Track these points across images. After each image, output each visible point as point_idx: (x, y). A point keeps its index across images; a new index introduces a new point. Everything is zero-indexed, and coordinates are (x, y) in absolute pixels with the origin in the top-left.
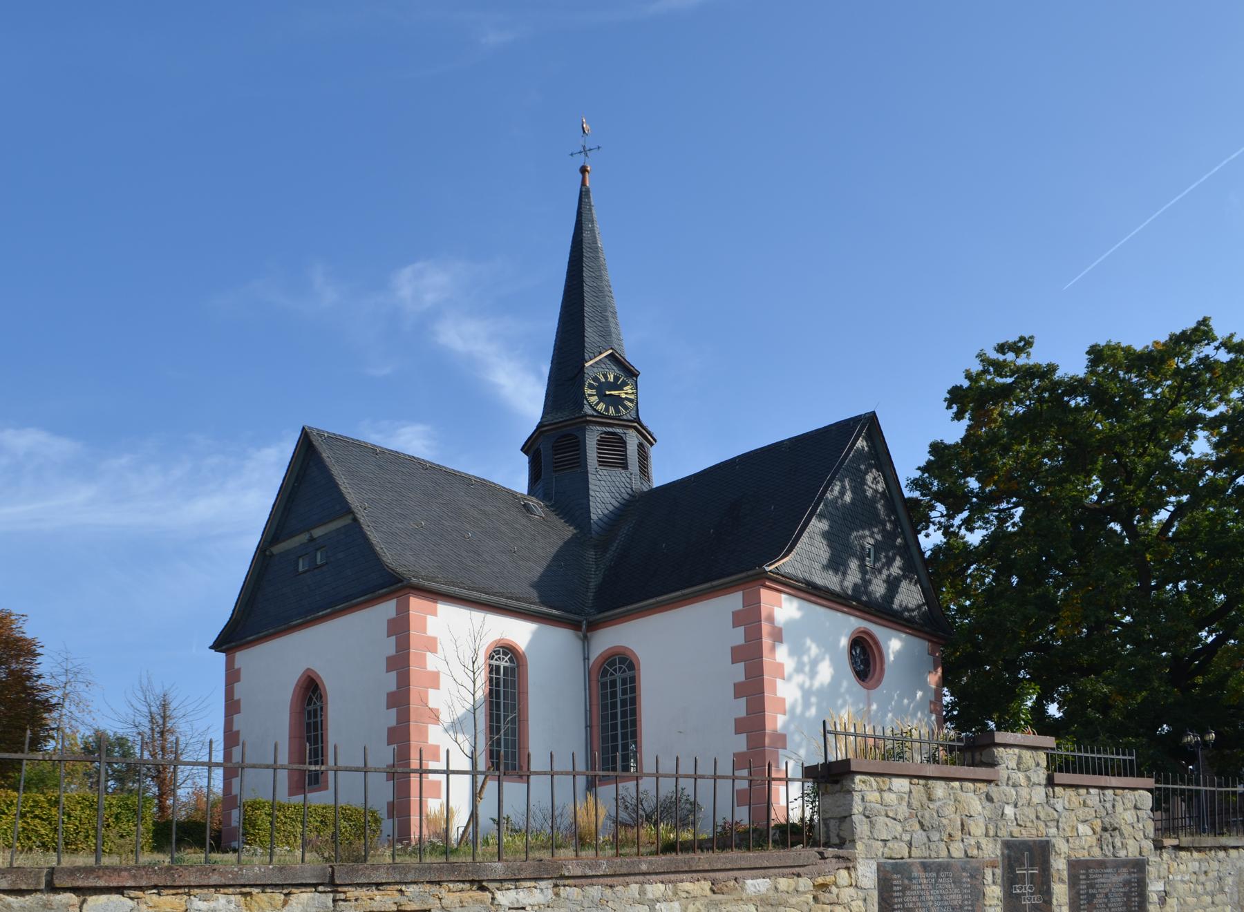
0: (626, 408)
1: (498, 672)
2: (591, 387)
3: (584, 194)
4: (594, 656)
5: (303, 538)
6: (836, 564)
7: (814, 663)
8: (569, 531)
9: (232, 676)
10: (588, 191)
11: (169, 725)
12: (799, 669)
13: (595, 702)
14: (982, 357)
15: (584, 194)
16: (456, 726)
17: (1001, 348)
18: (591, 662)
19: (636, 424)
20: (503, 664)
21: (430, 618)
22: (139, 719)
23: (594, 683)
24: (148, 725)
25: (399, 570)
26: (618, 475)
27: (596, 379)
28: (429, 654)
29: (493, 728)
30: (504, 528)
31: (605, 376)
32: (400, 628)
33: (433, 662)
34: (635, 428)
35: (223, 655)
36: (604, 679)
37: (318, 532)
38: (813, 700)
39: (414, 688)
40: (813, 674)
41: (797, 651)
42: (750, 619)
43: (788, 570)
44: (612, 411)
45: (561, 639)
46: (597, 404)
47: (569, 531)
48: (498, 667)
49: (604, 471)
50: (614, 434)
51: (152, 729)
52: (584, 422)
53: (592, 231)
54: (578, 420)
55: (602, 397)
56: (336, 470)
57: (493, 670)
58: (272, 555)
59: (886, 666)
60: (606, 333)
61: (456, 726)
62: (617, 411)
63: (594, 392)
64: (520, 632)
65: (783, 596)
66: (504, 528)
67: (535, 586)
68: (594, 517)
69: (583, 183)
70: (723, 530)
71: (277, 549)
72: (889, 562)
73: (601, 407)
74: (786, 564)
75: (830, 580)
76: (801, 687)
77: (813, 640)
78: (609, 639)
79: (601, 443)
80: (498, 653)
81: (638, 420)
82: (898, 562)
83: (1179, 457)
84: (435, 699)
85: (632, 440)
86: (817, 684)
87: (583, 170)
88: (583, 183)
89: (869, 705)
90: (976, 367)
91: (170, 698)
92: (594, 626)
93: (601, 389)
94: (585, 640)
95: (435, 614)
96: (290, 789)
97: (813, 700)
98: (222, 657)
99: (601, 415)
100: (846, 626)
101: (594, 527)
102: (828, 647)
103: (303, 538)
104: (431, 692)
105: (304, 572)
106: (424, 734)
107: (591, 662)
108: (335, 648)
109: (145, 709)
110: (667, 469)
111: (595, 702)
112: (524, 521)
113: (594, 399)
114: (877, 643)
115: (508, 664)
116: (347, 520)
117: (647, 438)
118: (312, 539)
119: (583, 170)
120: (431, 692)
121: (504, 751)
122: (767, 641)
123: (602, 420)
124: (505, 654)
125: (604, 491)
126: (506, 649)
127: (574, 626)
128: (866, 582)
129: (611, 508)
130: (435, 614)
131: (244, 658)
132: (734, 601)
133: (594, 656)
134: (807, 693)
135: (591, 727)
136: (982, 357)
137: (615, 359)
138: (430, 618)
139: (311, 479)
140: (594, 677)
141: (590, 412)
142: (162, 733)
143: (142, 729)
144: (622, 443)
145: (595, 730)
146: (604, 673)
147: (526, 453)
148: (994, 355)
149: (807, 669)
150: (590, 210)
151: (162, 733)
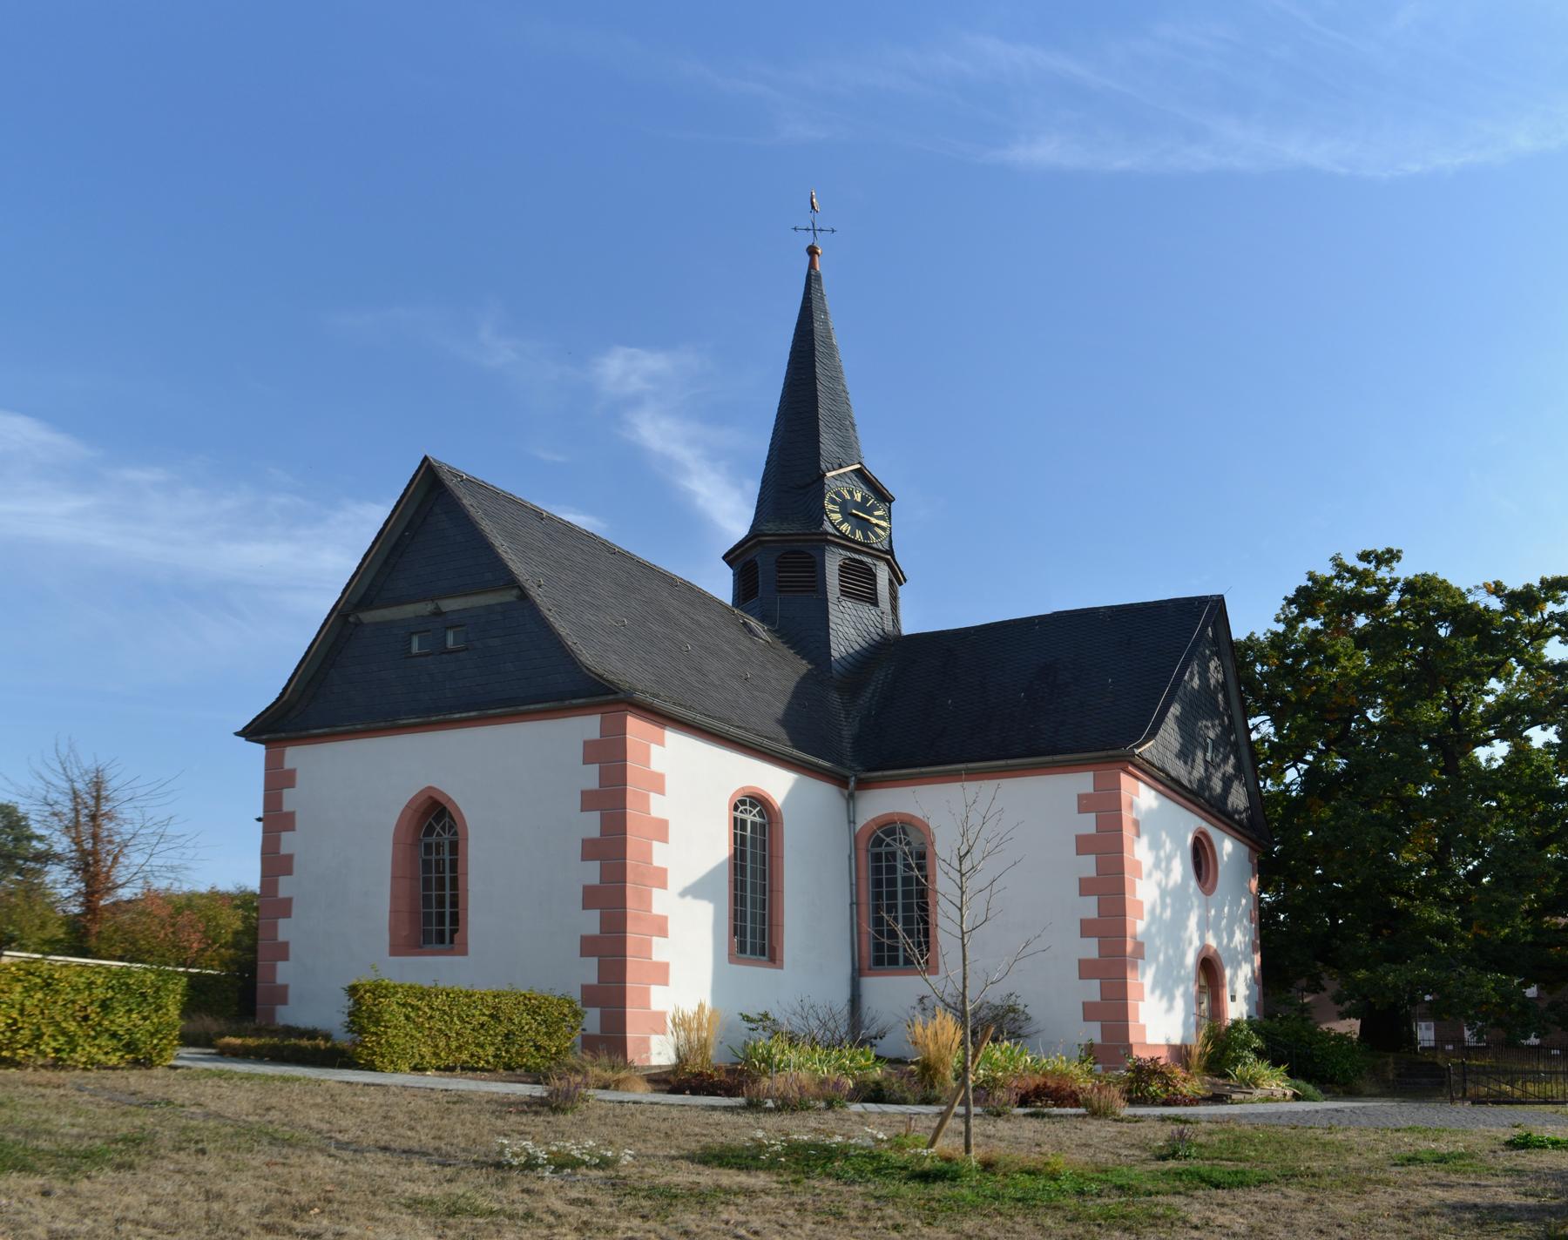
0: (877, 536)
1: (744, 828)
2: (833, 501)
3: (812, 280)
4: (861, 822)
5: (425, 608)
6: (1185, 754)
7: (1169, 859)
8: (803, 666)
9: (277, 781)
10: (818, 277)
11: (105, 808)
12: (1157, 865)
13: (863, 874)
14: (1337, 562)
15: (812, 280)
16: (696, 891)
17: (1364, 557)
18: (858, 827)
19: (888, 556)
20: (749, 818)
21: (654, 748)
22: (53, 796)
23: (862, 854)
24: (70, 805)
25: (611, 677)
26: (865, 611)
27: (838, 494)
28: (652, 795)
29: (738, 899)
30: (726, 647)
31: (850, 493)
32: (610, 758)
33: (658, 806)
34: (888, 562)
35: (263, 747)
36: (878, 850)
37: (449, 605)
38: (1168, 900)
39: (631, 839)
40: (1168, 872)
41: (1155, 845)
42: (1107, 809)
43: (1147, 756)
44: (859, 535)
45: (823, 793)
46: (841, 523)
47: (803, 666)
48: (744, 822)
49: (848, 604)
50: (861, 562)
51: (76, 811)
52: (824, 541)
53: (826, 323)
54: (798, 541)
55: (847, 516)
56: (486, 526)
57: (738, 824)
58: (359, 624)
59: (1220, 868)
60: (848, 445)
61: (696, 891)
62: (866, 537)
63: (836, 508)
64: (777, 782)
65: (1141, 785)
66: (726, 647)
67: (779, 721)
68: (835, 654)
69: (812, 265)
70: (1062, 690)
71: (368, 617)
72: (1225, 760)
73: (845, 528)
74: (1147, 749)
75: (1177, 769)
76: (1159, 885)
77: (1168, 834)
78: (883, 803)
79: (844, 569)
80: (743, 802)
81: (891, 552)
82: (1232, 760)
83: (1490, 699)
84: (660, 855)
85: (883, 574)
86: (1171, 883)
87: (812, 251)
88: (812, 265)
89: (1208, 911)
90: (1327, 571)
91: (112, 786)
92: (864, 785)
93: (844, 508)
94: (851, 798)
95: (661, 743)
96: (392, 945)
97: (1168, 900)
98: (258, 751)
99: (844, 536)
100: (1189, 823)
101: (835, 665)
102: (1177, 841)
103: (425, 608)
104: (656, 845)
105: (420, 655)
106: (647, 902)
107: (858, 827)
108: (501, 772)
109: (66, 785)
110: (921, 613)
111: (863, 874)
112: (747, 643)
113: (837, 517)
114: (1211, 845)
115: (757, 819)
116: (509, 596)
117: (897, 577)
118: (438, 613)
119: (812, 251)
120: (656, 845)
121: (753, 928)
122: (1128, 832)
123: (844, 542)
124: (753, 805)
125: (848, 627)
126: (755, 800)
127: (840, 781)
128: (1208, 778)
129: (857, 647)
130: (661, 743)
131: (296, 756)
132: (1083, 782)
133: (861, 822)
134: (1164, 893)
135: (858, 904)
136: (1337, 562)
137: (861, 474)
138: (654, 748)
139: (434, 529)
140: (862, 846)
141: (831, 530)
142: (93, 818)
143: (58, 808)
144: (872, 576)
145: (864, 908)
146: (878, 842)
147: (730, 563)
148: (1351, 561)
149: (1163, 865)
150: (822, 298)
151: (93, 818)
